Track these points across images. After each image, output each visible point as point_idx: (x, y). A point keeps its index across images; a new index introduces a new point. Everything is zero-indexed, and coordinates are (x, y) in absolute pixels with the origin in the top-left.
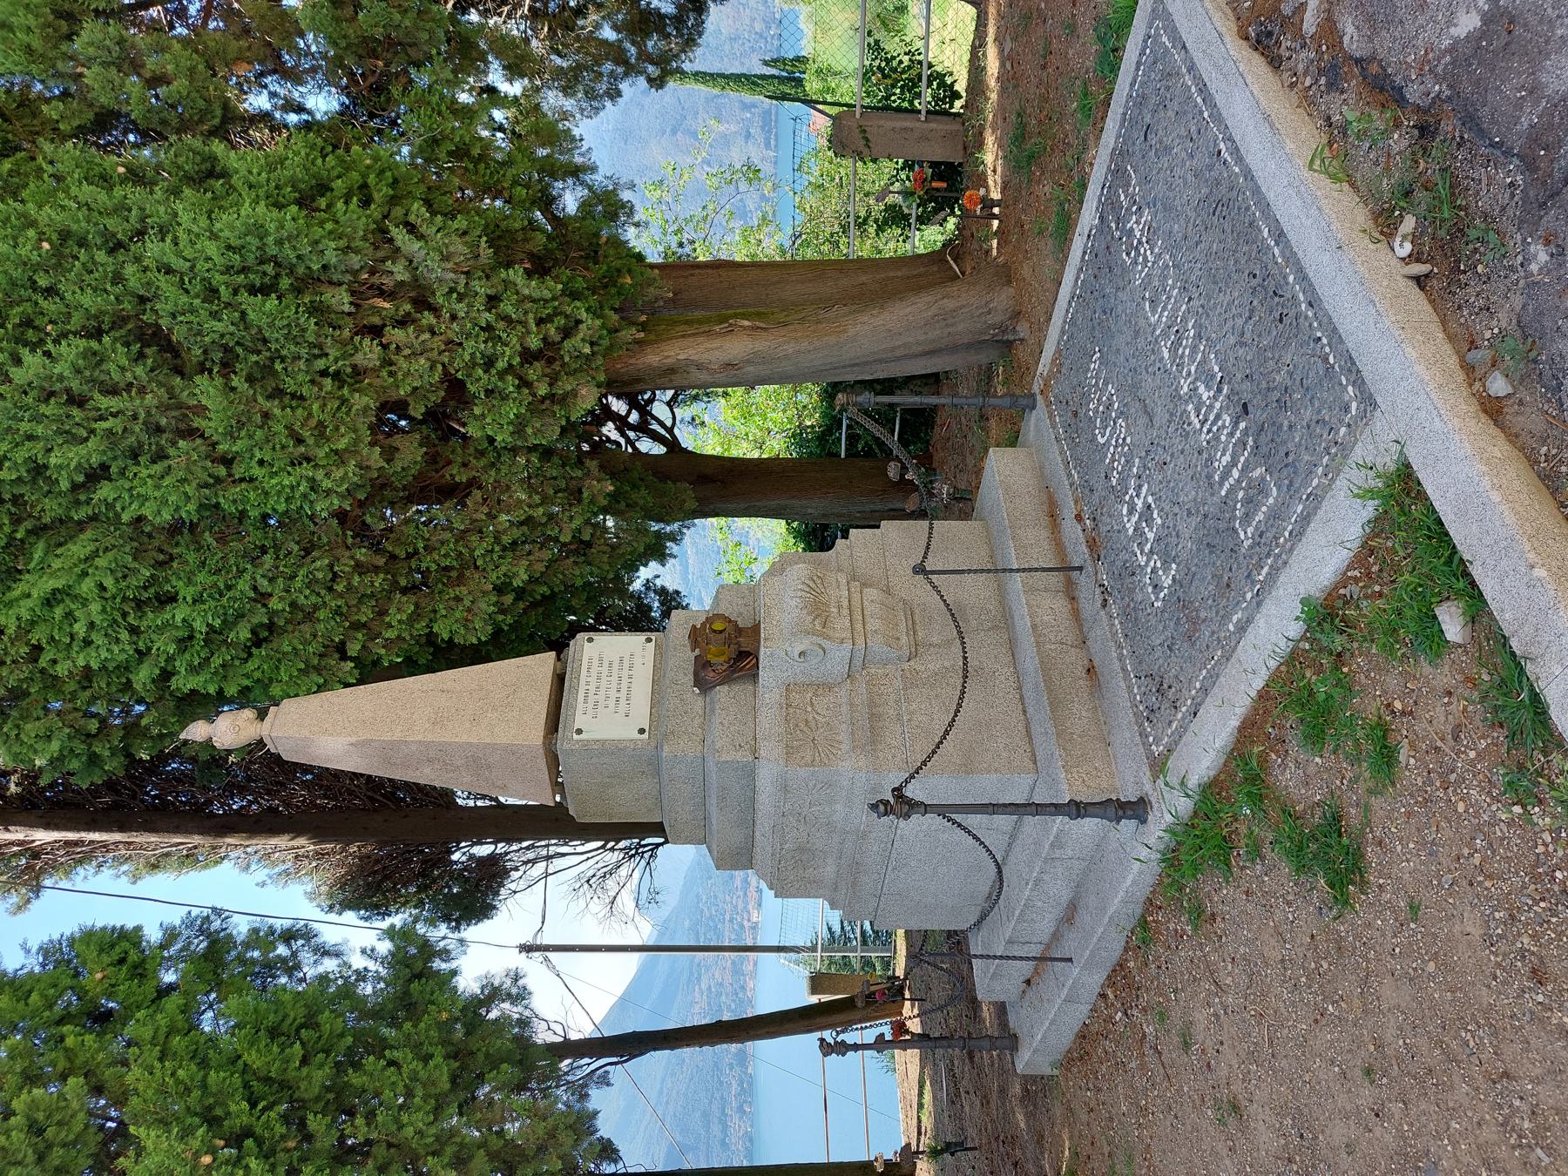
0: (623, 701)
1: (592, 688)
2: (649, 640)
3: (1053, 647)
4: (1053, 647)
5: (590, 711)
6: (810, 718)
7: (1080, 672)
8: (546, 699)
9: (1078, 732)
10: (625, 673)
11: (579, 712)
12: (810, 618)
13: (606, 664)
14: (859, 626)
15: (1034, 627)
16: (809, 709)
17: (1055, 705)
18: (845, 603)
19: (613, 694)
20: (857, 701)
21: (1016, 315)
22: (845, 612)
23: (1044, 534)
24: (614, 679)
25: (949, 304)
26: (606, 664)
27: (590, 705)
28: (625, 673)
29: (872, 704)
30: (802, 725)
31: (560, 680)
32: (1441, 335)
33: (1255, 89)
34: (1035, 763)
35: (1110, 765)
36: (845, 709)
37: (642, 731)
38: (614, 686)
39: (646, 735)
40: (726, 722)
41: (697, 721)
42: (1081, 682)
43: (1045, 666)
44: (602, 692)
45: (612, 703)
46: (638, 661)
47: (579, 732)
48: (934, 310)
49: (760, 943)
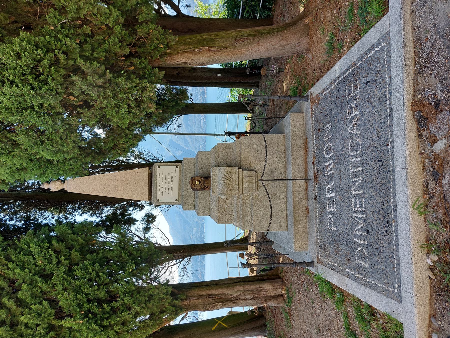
0: (170, 190)
1: (161, 185)
2: (177, 167)
3: (298, 199)
4: (298, 199)
5: (161, 193)
6: (225, 207)
7: (304, 209)
8: (147, 185)
9: (300, 230)
10: (170, 180)
11: (158, 194)
12: (226, 189)
13: (164, 176)
14: (241, 187)
15: (293, 192)
16: (225, 204)
17: (295, 220)
18: (237, 179)
19: (167, 187)
20: (239, 203)
21: (308, 50)
22: (237, 183)
23: (302, 153)
24: (167, 182)
25: (284, 42)
26: (164, 176)
27: (161, 191)
28: (170, 180)
29: (243, 206)
30: (223, 210)
31: (151, 176)
32: (428, 302)
33: (407, 148)
34: (287, 227)
35: (307, 241)
36: (235, 205)
37: (176, 200)
38: (167, 184)
39: (178, 201)
40: (201, 203)
41: (192, 199)
42: (304, 213)
43: (294, 207)
44: (164, 187)
45: (167, 190)
46: (174, 175)
47: (158, 200)
48: (278, 45)
49: (207, 133)
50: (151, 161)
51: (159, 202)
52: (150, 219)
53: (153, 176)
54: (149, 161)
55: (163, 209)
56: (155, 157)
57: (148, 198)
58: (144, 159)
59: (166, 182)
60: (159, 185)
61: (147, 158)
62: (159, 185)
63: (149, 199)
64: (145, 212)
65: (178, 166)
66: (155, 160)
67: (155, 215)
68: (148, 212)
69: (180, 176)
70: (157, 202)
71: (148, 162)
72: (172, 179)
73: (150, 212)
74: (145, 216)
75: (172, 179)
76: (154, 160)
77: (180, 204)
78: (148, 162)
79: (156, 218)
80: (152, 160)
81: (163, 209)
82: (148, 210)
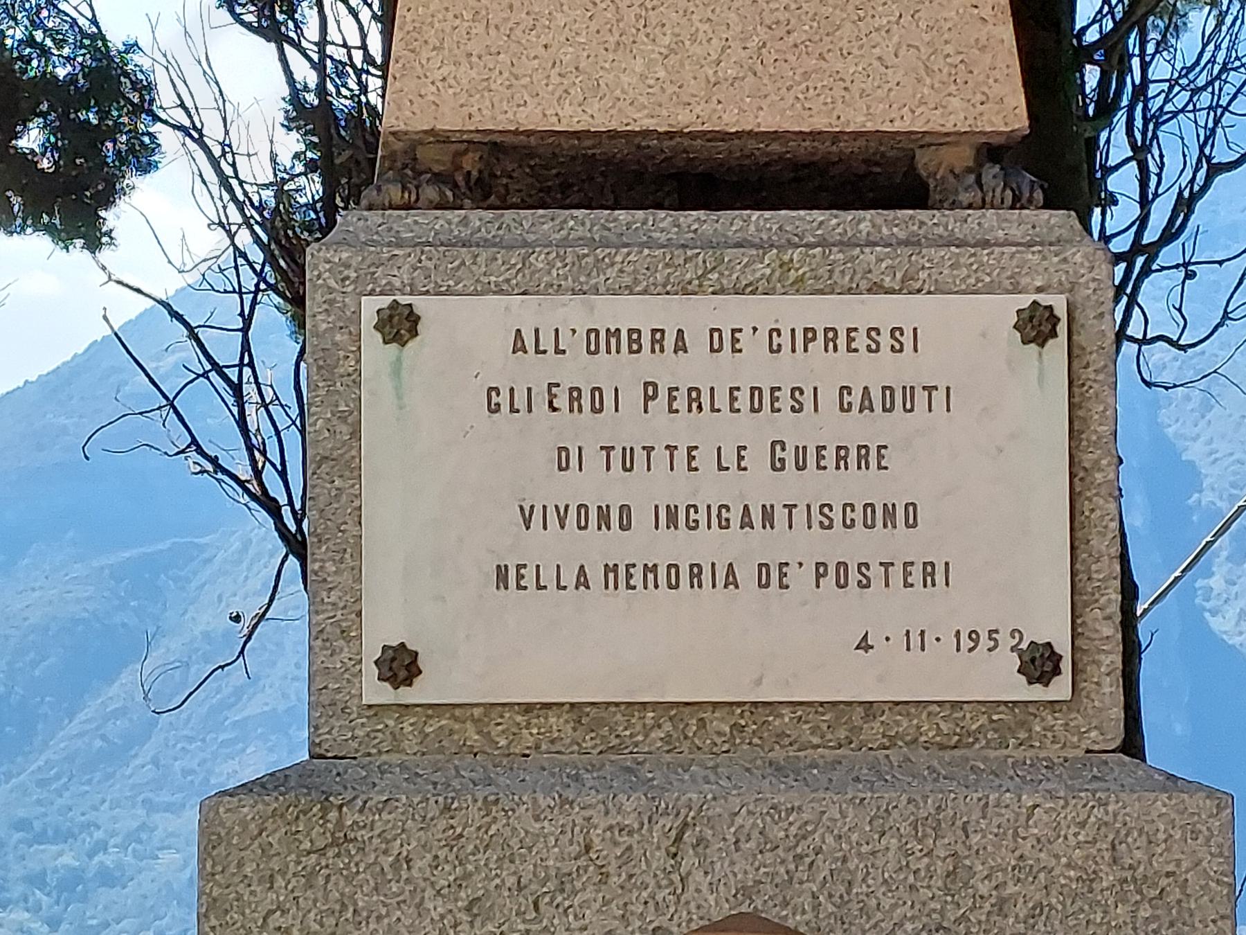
8: (685, 119)
39: (375, 691)
50: (1117, 146)
51: (371, 339)
52: (31, 139)
53: (866, 221)
54: (1106, 108)
55: (226, 350)
56: (1186, 204)
57: (440, 138)
58: (1153, 55)
59: (758, 458)
60: (698, 342)
61: (1161, 69)
62: (698, 342)
63: (431, 156)
64: (169, 36)
65: (1060, 689)
66: (1123, 214)
67: (111, 217)
68: (165, 97)
69: (873, 731)
70: (371, 306)
71: (1092, 76)
72: (802, 578)
73: (167, 137)
74: (95, 40)
75: (802, 578)
76: (1123, 182)
77: (337, 735)
78: (1092, 76)
79: (63, 237)
80: (1140, 152)
81: (226, 350)
82: (204, 96)
